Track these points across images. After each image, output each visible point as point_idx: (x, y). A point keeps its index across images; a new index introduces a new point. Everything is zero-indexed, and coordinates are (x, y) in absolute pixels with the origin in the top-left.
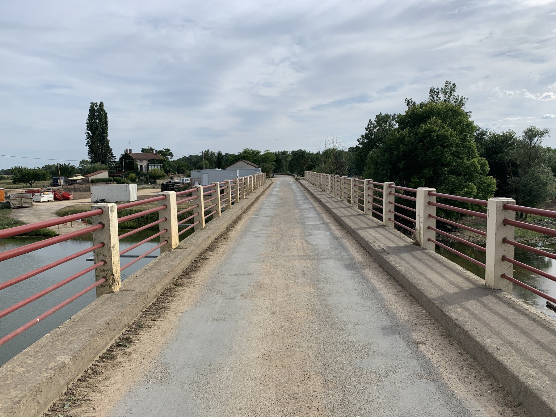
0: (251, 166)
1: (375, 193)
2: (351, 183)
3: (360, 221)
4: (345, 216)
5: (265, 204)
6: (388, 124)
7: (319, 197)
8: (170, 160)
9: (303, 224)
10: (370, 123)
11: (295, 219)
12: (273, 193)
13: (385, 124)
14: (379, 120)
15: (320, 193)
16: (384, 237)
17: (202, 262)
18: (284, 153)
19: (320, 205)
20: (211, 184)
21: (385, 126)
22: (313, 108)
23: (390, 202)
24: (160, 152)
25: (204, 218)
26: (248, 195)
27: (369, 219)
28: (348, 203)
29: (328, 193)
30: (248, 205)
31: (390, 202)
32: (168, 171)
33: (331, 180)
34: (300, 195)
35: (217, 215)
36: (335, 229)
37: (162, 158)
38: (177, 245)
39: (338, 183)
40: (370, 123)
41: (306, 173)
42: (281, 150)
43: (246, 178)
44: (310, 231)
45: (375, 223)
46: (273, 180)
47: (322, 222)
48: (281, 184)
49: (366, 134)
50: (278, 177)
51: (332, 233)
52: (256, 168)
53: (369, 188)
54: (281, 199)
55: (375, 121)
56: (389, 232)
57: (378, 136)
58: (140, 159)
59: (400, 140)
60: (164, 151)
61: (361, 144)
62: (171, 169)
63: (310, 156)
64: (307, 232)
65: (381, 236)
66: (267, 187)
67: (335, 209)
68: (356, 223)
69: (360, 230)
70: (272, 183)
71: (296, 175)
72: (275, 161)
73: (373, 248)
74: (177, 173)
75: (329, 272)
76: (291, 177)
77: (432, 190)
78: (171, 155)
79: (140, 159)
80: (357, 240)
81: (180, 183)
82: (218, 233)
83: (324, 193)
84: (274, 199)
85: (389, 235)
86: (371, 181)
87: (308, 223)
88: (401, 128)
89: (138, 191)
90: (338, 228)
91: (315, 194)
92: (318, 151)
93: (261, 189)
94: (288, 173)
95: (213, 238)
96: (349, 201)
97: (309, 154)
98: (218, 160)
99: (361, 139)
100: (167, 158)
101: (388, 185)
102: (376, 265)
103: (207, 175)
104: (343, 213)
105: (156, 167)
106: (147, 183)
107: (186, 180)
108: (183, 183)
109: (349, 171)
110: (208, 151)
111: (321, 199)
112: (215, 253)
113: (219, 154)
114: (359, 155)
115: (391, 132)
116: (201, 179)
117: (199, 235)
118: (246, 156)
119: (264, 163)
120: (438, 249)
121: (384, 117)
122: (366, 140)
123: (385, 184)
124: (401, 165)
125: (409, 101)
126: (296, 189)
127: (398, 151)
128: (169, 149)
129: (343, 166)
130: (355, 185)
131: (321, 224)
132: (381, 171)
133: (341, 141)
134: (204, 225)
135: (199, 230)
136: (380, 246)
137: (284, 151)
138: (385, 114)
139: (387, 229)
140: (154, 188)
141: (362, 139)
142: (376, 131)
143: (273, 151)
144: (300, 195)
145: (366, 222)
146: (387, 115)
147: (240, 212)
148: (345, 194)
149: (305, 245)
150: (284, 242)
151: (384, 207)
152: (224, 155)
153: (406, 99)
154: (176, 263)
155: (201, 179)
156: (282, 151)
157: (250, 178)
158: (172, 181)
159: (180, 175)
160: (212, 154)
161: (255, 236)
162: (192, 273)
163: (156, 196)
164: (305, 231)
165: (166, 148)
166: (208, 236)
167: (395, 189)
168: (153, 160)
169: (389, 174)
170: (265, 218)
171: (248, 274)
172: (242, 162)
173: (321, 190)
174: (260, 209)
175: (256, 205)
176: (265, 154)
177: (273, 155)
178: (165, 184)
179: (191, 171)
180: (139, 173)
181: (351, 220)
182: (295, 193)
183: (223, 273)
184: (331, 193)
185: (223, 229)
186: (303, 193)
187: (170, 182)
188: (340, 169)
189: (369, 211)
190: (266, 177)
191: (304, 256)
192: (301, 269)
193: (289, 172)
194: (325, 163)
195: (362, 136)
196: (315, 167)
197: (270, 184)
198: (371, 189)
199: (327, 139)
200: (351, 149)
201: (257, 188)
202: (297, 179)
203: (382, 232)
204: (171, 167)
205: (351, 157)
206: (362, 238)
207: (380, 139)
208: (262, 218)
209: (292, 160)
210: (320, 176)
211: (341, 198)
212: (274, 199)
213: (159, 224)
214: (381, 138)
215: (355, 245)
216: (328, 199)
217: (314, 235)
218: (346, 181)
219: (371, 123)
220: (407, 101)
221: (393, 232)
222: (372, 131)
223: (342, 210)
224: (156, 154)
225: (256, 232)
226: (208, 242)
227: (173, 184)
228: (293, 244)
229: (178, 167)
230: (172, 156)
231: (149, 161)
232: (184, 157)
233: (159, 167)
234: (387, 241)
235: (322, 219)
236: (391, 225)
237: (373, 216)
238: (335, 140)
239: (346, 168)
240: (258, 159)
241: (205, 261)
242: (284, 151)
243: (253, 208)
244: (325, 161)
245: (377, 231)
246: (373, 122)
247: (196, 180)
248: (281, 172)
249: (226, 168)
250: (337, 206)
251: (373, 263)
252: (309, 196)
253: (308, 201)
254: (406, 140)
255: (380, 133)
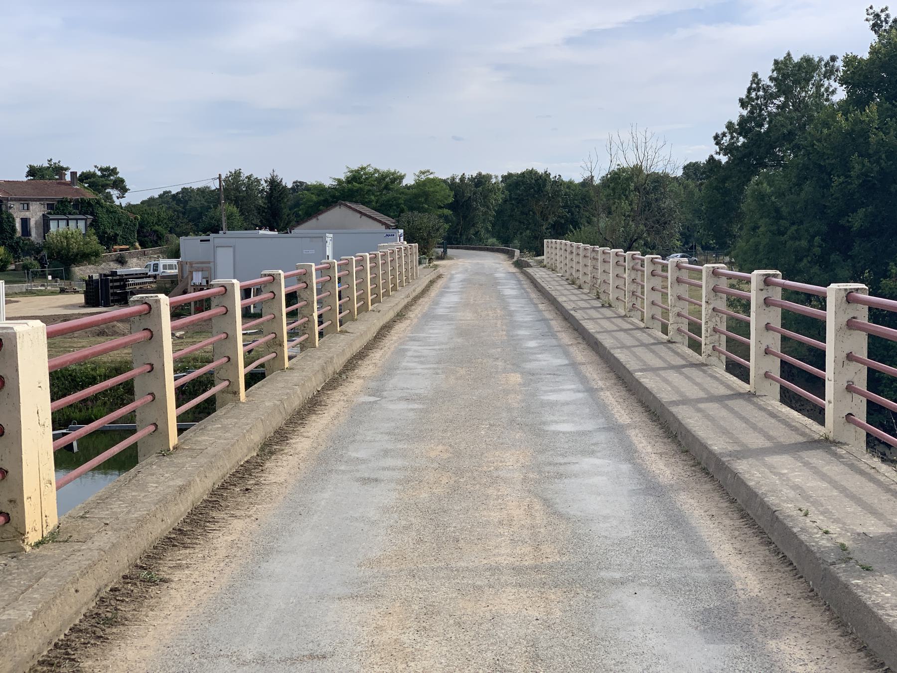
0: (370, 221)
1: (790, 320)
2: (704, 283)
3: (738, 424)
4: (685, 401)
5: (409, 354)
6: (811, 89)
7: (590, 327)
8: (117, 202)
9: (537, 431)
10: (754, 86)
11: (509, 410)
12: (440, 311)
13: (803, 89)
14: (785, 76)
15: (594, 313)
16: (835, 493)
17: (142, 598)
18: (481, 181)
19: (596, 358)
20: (321, 264)
21: (803, 94)
22: (570, 41)
23: (850, 357)
24: (85, 177)
25: (242, 372)
26: (353, 320)
27: (773, 415)
28: (690, 352)
29: (623, 313)
30: (348, 355)
31: (850, 357)
32: (109, 238)
33: (633, 269)
34: (528, 318)
35: (230, 396)
36: (649, 449)
37: (90, 195)
38: (50, 528)
39: (657, 282)
40: (754, 86)
41: (549, 244)
42: (471, 172)
43: (347, 264)
44: (561, 460)
45: (795, 429)
46: (445, 266)
47: (601, 421)
48: (467, 282)
49: (743, 121)
50: (458, 257)
51: (641, 471)
52: (388, 227)
53: (767, 302)
54: (463, 332)
55: (771, 79)
56: (852, 467)
57: (782, 126)
58: (20, 200)
59: (854, 139)
60: (99, 173)
61: (726, 150)
62: (120, 232)
63: (564, 190)
64: (550, 464)
65: (825, 485)
66: (419, 290)
67: (649, 374)
68: (725, 432)
69: (745, 461)
70: (440, 277)
71: (517, 252)
72: (450, 206)
73: (802, 542)
74: (137, 244)
75: (634, 650)
76: (502, 256)
77: (857, 290)
78: (120, 185)
79: (20, 200)
80: (733, 501)
81: (146, 276)
82: (227, 466)
83: (607, 312)
84: (439, 332)
85: (854, 482)
86: (775, 276)
87: (553, 428)
88: (856, 102)
89: (7, 302)
90: (660, 447)
91: (578, 315)
92: (587, 175)
93: (399, 299)
94: (493, 245)
95: (200, 489)
96: (695, 346)
97: (558, 183)
98: (270, 202)
99: (724, 135)
100: (109, 197)
101: (844, 294)
102: (819, 618)
103: (231, 249)
104: (677, 390)
105: (72, 224)
106: (44, 276)
107: (165, 267)
108: (155, 277)
109: (686, 237)
110: (237, 174)
111: (598, 336)
112: (198, 553)
113: (274, 183)
114: (717, 188)
115: (822, 115)
116: (212, 265)
117: (149, 478)
118: (357, 191)
119: (416, 213)
120: (872, 443)
121: (799, 65)
122: (742, 140)
123: (834, 291)
124: (857, 220)
125: (877, 16)
126: (516, 297)
127: (846, 177)
128: (115, 169)
129: (665, 223)
130: (715, 290)
131: (599, 430)
132: (793, 238)
133: (661, 143)
134: (173, 438)
135: (153, 458)
136: (826, 532)
137: (480, 174)
138: (801, 56)
139: (841, 457)
140: (63, 291)
141: (728, 137)
142: (772, 109)
143: (443, 173)
144: (528, 318)
145: (760, 425)
146: (808, 60)
147: (315, 383)
148: (679, 319)
149: (540, 517)
150: (464, 505)
151: (752, 342)
152: (290, 186)
153: (871, 11)
154: (22, 612)
155: (212, 265)
156: (474, 175)
157: (361, 262)
158: (121, 271)
159: (149, 250)
160: (252, 183)
161: (357, 480)
162: (92, 651)
163: (66, 318)
164: (541, 458)
165: (105, 166)
166: (179, 482)
167: (870, 309)
168: (62, 202)
169: (817, 250)
170: (403, 405)
171: (312, 657)
172: (343, 208)
173: (597, 304)
174: (389, 370)
175: (376, 356)
176: (420, 185)
177: (445, 186)
178: (97, 281)
179: (182, 239)
180: (17, 243)
181: (708, 417)
182: (511, 314)
183: (212, 651)
184: (632, 313)
185: (244, 452)
186: (540, 311)
187: (114, 274)
188: (658, 232)
189: (767, 383)
190: (416, 257)
191: (536, 568)
192: (522, 632)
193: (494, 240)
194: (610, 213)
195: (730, 126)
196: (576, 225)
197: (432, 282)
198: (723, 292)
199: (615, 137)
200: (691, 169)
201: (386, 294)
202: (519, 265)
203: (826, 469)
204: (120, 224)
205: (691, 194)
206: (752, 494)
207: (789, 137)
208: (392, 406)
209: (505, 201)
210: (594, 254)
211: (665, 331)
212: (439, 332)
213: (132, 380)
214: (790, 133)
215: (727, 522)
216: (622, 335)
217: (576, 476)
218: (684, 275)
219: (758, 84)
220: (871, 17)
221: (868, 470)
222: (761, 110)
223: (673, 376)
224: (72, 183)
225: (363, 461)
226: (183, 507)
227: (123, 279)
228: (495, 516)
229: (142, 226)
230: (124, 190)
231: (50, 206)
232: (165, 195)
233: (82, 224)
234: (851, 508)
235: (602, 410)
236: (856, 440)
237: (728, 370)
238: (641, 140)
239: (676, 228)
240: (395, 199)
241: (153, 590)
242: (480, 174)
243: (366, 369)
244: (609, 208)
245: (806, 464)
246: (766, 81)
247: (194, 267)
248: (469, 240)
249: (292, 228)
250: (654, 361)
251: (805, 605)
252: (557, 324)
253: (554, 342)
254: (873, 139)
255: (787, 118)
